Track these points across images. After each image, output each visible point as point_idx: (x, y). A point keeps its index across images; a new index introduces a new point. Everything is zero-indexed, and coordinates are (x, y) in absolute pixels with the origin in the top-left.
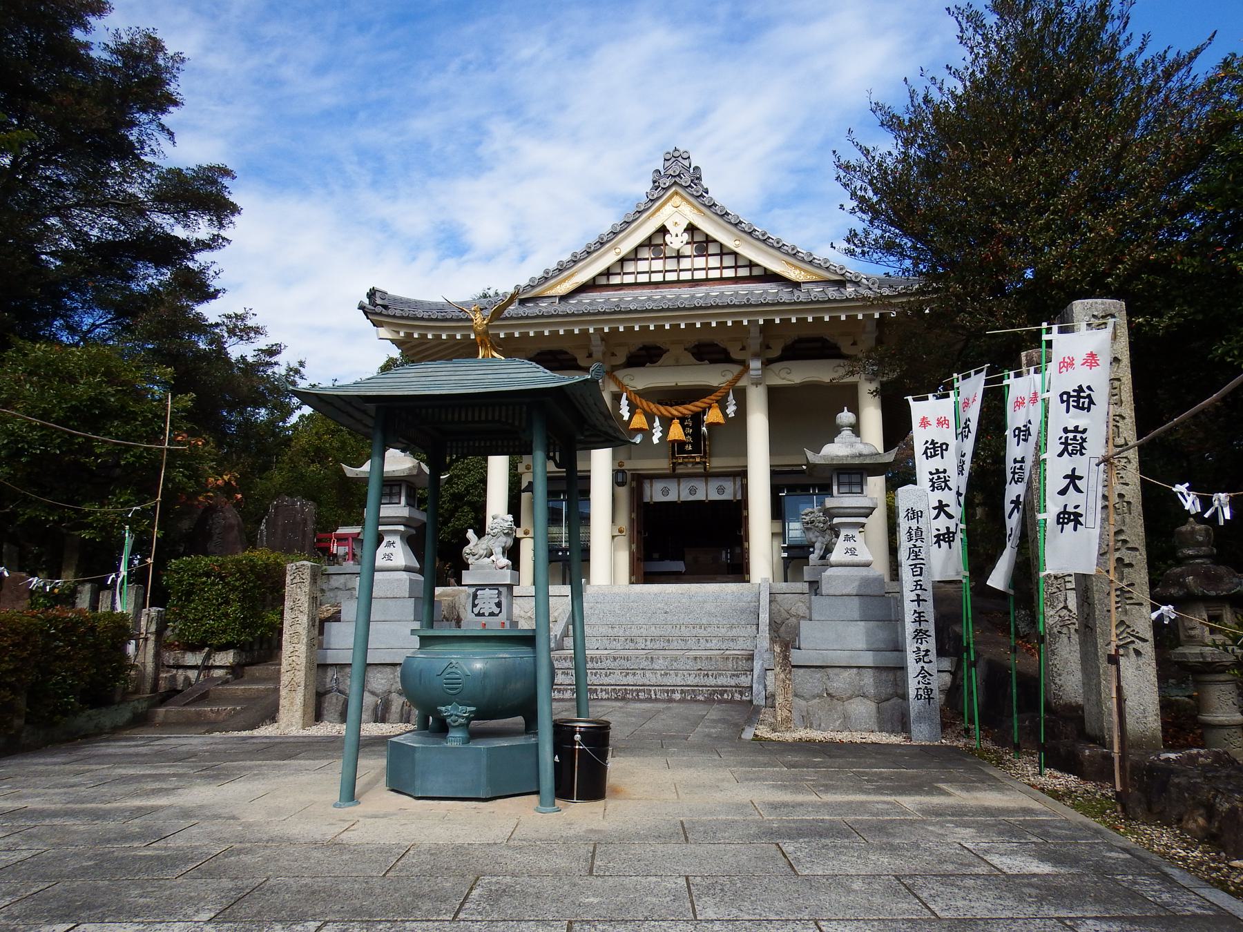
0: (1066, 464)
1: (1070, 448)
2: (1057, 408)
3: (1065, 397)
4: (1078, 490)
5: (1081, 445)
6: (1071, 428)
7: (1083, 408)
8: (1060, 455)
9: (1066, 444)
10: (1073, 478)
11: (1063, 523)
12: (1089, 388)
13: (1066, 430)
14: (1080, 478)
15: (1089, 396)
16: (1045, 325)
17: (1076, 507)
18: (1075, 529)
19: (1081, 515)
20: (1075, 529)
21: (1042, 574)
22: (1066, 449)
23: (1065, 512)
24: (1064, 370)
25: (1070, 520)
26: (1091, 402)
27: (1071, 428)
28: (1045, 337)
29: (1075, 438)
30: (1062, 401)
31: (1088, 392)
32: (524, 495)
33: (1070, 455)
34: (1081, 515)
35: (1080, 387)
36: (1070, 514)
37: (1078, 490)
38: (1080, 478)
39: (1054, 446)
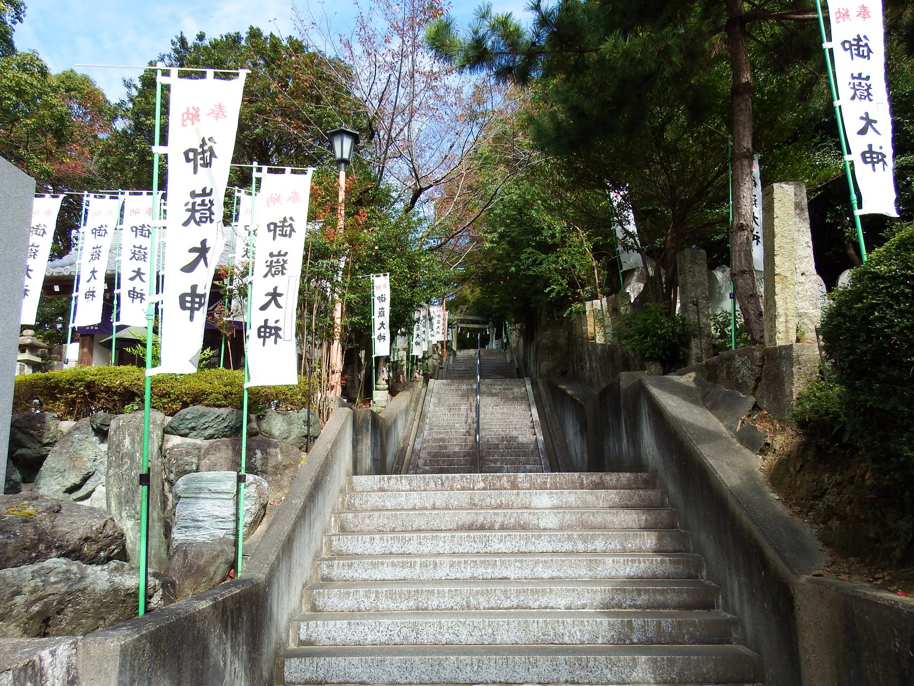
0: (270, 284)
1: (198, 215)
2: (263, 232)
3: (272, 227)
4: (279, 306)
5: (283, 266)
6: (276, 253)
7: (285, 236)
8: (186, 224)
9: (193, 210)
10: (275, 295)
11: (265, 337)
12: (291, 219)
13: (271, 255)
14: (280, 295)
15: (291, 225)
16: (255, 164)
17: (277, 322)
18: (276, 342)
19: (280, 329)
20: (276, 342)
21: (373, 356)
22: (192, 217)
23: (266, 326)
24: (272, 204)
25: (271, 335)
26: (292, 230)
27: (276, 253)
28: (255, 174)
29: (278, 261)
30: (270, 230)
31: (290, 222)
32: (32, 321)
33: (198, 223)
34: (280, 329)
35: (285, 218)
36: (271, 328)
37: (279, 306)
38: (280, 295)
39: (260, 268)
